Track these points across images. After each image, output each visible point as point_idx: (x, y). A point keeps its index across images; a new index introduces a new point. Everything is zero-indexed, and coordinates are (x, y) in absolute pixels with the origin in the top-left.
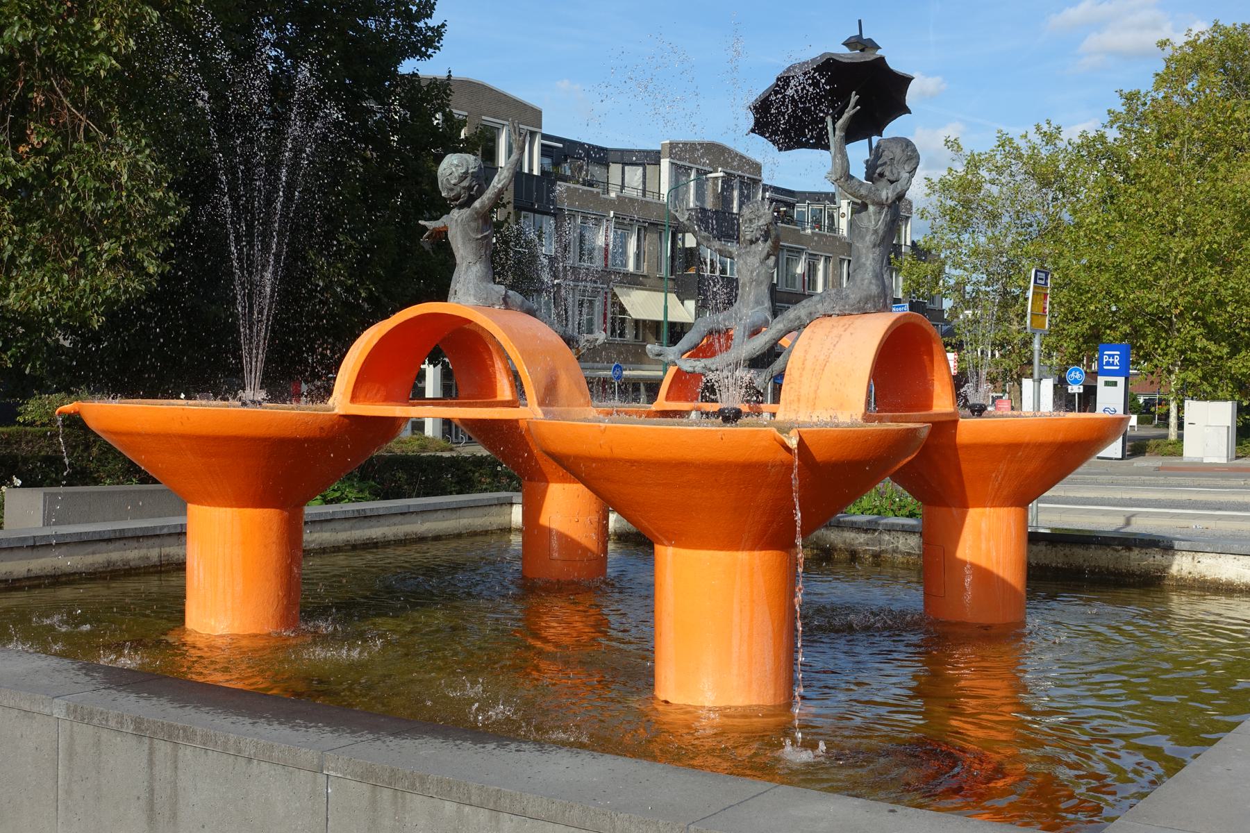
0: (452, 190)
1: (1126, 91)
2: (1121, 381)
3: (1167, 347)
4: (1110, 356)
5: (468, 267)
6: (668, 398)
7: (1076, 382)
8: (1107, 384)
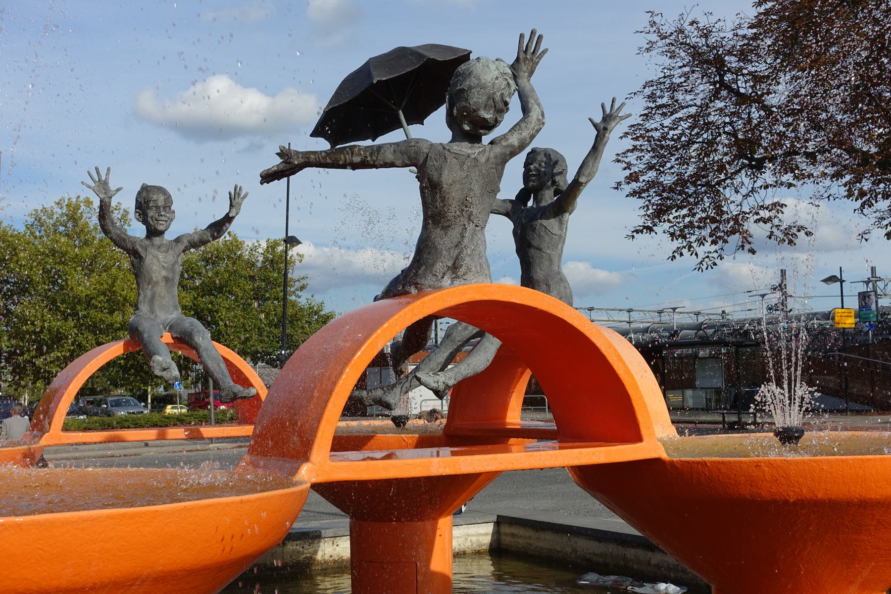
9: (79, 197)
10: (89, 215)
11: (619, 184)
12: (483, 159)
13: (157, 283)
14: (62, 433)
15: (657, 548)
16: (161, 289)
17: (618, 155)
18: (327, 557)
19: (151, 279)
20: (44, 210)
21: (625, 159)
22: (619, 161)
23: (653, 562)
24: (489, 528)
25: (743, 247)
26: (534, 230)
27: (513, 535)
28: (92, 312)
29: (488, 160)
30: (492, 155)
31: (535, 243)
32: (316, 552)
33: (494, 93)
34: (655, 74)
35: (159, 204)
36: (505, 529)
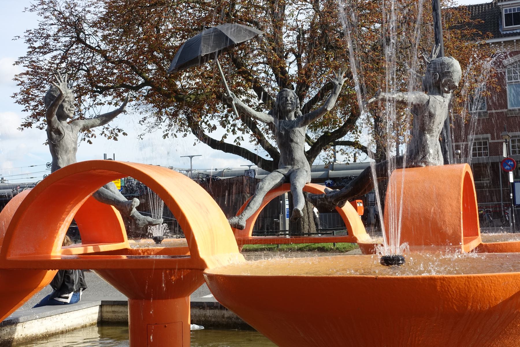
11: (16, 94)
15: (224, 308)
17: (16, 75)
18: (19, 336)
19: (67, 148)
21: (19, 79)
22: (16, 79)
23: (226, 316)
24: (97, 309)
25: (84, 139)
26: (294, 133)
27: (114, 312)
31: (295, 140)
32: (14, 332)
34: (34, 26)
36: (106, 309)
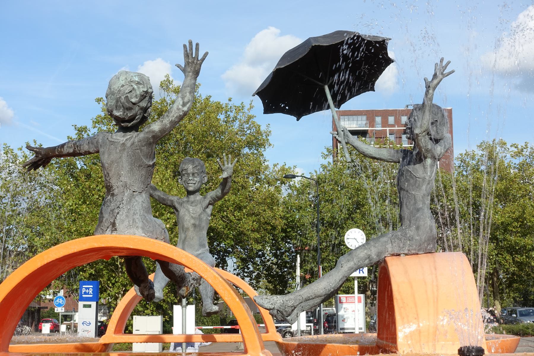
0: (129, 109)
1: (79, 126)
2: (94, 304)
3: (116, 282)
4: (86, 288)
5: (132, 197)
6: (117, 331)
7: (59, 305)
8: (85, 306)
9: (494, 140)
10: (504, 154)
12: (129, 144)
13: (188, 229)
14: (114, 335)
16: (191, 233)
19: (183, 226)
20: (467, 154)
28: (508, 236)
29: (133, 144)
30: (136, 140)
33: (120, 97)
35: (189, 172)
